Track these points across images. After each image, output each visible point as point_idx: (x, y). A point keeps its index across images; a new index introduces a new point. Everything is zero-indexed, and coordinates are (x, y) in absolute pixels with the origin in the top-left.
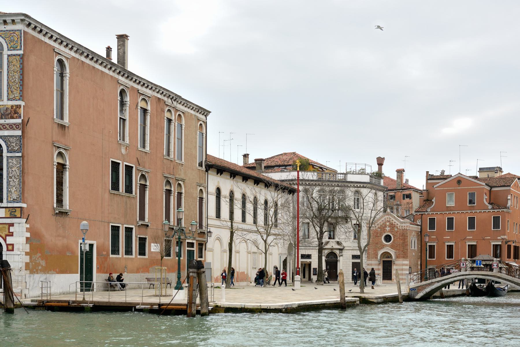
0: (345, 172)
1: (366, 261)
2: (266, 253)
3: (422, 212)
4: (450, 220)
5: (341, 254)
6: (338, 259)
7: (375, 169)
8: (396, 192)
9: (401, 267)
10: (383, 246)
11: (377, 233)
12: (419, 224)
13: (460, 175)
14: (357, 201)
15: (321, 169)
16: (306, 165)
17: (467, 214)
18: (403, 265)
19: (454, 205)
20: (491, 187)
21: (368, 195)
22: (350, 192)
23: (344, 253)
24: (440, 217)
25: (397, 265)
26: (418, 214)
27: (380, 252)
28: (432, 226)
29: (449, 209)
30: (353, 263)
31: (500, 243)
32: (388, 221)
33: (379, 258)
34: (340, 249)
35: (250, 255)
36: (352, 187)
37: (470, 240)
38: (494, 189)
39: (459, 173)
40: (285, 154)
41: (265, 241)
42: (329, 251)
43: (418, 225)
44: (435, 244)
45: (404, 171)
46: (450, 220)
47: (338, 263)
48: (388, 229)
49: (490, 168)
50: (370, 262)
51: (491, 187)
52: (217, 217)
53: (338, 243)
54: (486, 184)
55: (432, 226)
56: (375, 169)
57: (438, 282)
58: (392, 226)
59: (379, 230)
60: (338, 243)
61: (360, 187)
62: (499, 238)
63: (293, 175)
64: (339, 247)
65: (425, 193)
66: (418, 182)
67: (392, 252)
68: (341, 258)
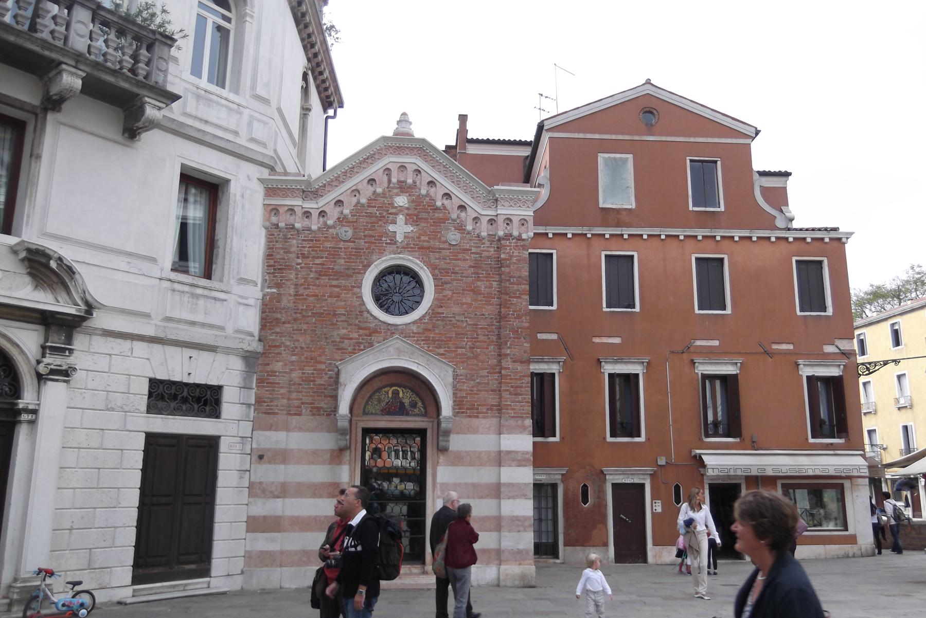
1: (246, 428)
4: (620, 267)
5: (53, 361)
6: (27, 399)
9: (486, 475)
10: (369, 336)
11: (334, 254)
13: (649, 90)
18: (500, 459)
19: (633, 206)
23: (87, 353)
24: (575, 250)
25: (459, 459)
27: (356, 372)
29: (612, 217)
30: (153, 441)
31: (834, 372)
32: (403, 187)
33: (344, 408)
34: (46, 320)
37: (710, 354)
39: (648, 82)
44: (554, 368)
46: (620, 267)
47: (22, 435)
48: (401, 228)
59: (347, 232)
62: (829, 349)
64: (44, 300)
68: (54, 391)
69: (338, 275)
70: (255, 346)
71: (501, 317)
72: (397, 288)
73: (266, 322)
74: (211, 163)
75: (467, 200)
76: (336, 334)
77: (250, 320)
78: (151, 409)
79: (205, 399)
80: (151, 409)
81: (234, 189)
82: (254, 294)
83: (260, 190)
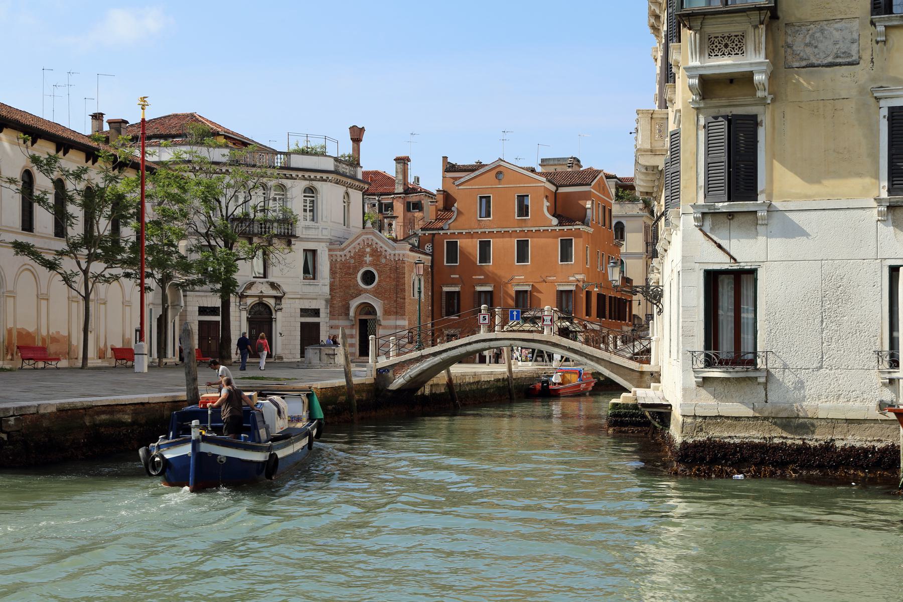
0: (286, 151)
2: (86, 298)
3: (433, 229)
5: (278, 307)
7: (347, 148)
8: (383, 194)
10: (359, 293)
11: (349, 268)
12: (428, 251)
14: (312, 209)
15: (241, 143)
16: (209, 134)
17: (514, 234)
20: (557, 187)
21: (330, 195)
22: (296, 188)
25: (385, 327)
26: (427, 233)
27: (354, 304)
28: (452, 257)
30: (302, 324)
32: (368, 245)
34: (275, 297)
35: (74, 305)
36: (300, 179)
38: (562, 190)
40: (176, 116)
41: (85, 272)
42: (256, 300)
43: (426, 254)
45: (408, 159)
48: (368, 259)
49: (559, 159)
50: (336, 322)
51: (557, 187)
52: (23, 229)
53: (273, 285)
54: (549, 181)
55: (452, 257)
56: (347, 148)
57: (435, 354)
58: (376, 253)
59: (352, 261)
60: (273, 285)
61: (315, 179)
63: (184, 151)
65: (440, 198)
66: (431, 180)
67: (378, 305)
68: (279, 313)
69: (350, 274)
70: (329, 297)
71: (397, 285)
72: (368, 278)
73: (331, 290)
74: (311, 246)
75: (387, 249)
76: (350, 292)
77: (327, 289)
78: (200, 314)
79: (316, 313)
80: (200, 314)
81: (319, 252)
82: (327, 281)
83: (327, 250)
